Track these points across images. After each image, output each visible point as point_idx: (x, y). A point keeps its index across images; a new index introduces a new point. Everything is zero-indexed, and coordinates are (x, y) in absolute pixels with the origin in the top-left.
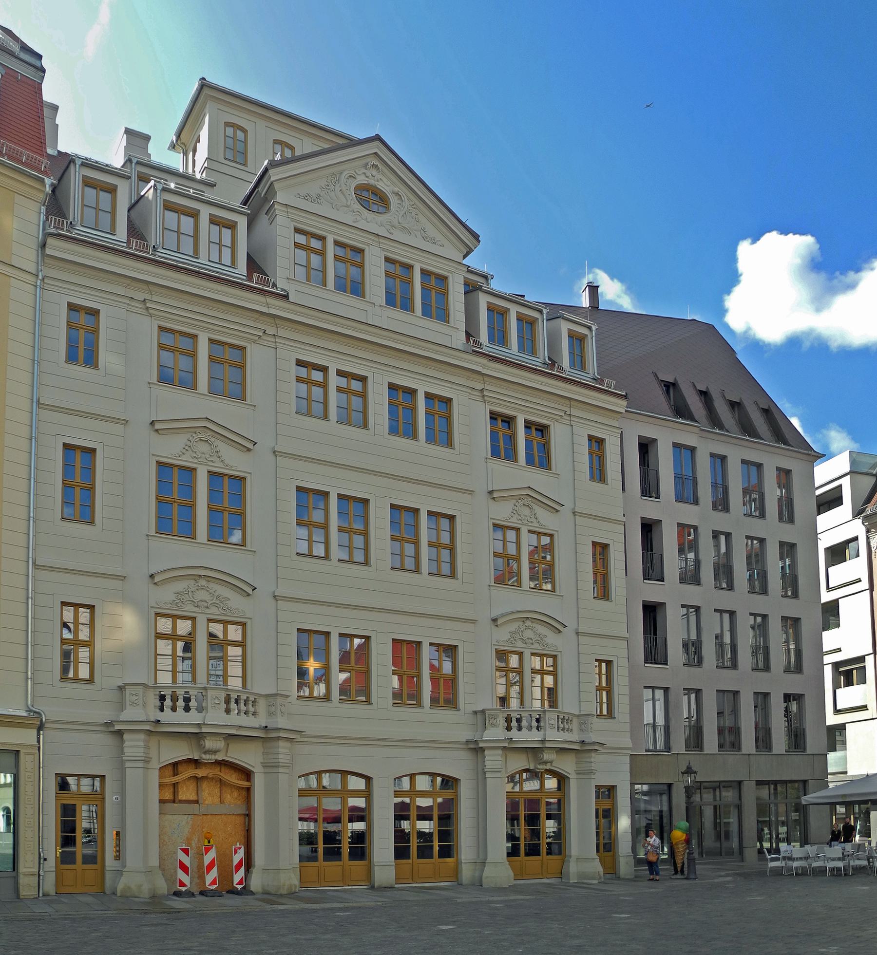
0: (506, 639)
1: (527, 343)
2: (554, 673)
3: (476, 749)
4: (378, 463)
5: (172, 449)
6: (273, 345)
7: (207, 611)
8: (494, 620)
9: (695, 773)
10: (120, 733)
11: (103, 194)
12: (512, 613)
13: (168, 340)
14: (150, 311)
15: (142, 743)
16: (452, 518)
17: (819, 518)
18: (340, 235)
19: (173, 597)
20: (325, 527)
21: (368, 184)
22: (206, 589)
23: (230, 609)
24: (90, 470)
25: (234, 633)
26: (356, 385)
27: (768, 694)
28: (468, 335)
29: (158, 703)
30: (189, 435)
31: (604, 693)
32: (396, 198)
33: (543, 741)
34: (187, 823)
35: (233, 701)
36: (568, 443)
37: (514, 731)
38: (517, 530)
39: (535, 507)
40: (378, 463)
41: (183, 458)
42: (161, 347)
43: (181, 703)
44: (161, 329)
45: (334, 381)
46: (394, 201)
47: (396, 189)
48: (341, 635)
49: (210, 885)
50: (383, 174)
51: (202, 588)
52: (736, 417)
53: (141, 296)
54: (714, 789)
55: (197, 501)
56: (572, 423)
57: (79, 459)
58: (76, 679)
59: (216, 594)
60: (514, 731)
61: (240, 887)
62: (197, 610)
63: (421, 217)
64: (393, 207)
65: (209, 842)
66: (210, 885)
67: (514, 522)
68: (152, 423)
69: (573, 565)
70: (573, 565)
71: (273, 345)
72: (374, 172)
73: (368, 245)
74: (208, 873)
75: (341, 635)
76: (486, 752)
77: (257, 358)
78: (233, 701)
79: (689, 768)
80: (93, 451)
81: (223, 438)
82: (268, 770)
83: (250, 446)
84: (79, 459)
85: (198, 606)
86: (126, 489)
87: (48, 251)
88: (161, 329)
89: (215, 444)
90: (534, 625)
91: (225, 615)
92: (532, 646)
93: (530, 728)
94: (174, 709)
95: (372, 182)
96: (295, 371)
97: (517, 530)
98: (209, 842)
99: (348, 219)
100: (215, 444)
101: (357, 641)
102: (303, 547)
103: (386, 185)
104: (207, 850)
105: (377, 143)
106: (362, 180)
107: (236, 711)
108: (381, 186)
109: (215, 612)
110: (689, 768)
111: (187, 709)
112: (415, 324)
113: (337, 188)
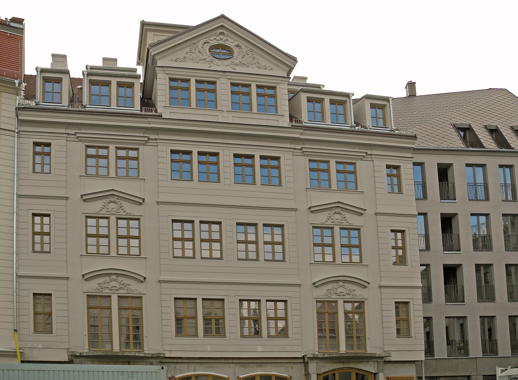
0: (324, 294)
6: (370, 159)
7: (344, 297)
8: (314, 284)
11: (339, 107)
13: (314, 165)
14: (80, 138)
16: (282, 226)
18: (171, 74)
19: (97, 286)
20: (332, 245)
22: (343, 287)
23: (131, 290)
26: (394, 172)
27: (493, 317)
28: (291, 118)
30: (329, 212)
32: (238, 48)
38: (332, 228)
39: (344, 213)
42: (311, 170)
44: (310, 161)
45: (258, 162)
46: (236, 51)
47: (237, 43)
48: (203, 299)
50: (228, 36)
51: (341, 286)
52: (494, 136)
53: (299, 147)
56: (373, 159)
59: (349, 288)
62: (111, 292)
63: (256, 56)
64: (235, 55)
67: (329, 223)
68: (309, 208)
71: (370, 159)
72: (221, 37)
73: (278, 83)
75: (203, 299)
77: (362, 166)
83: (141, 201)
87: (20, 118)
88: (310, 161)
89: (343, 214)
90: (345, 284)
91: (128, 293)
92: (344, 297)
95: (221, 42)
96: (386, 171)
97: (332, 228)
100: (120, 203)
101: (356, 304)
102: (319, 258)
103: (231, 43)
108: (227, 43)
113: (197, 51)
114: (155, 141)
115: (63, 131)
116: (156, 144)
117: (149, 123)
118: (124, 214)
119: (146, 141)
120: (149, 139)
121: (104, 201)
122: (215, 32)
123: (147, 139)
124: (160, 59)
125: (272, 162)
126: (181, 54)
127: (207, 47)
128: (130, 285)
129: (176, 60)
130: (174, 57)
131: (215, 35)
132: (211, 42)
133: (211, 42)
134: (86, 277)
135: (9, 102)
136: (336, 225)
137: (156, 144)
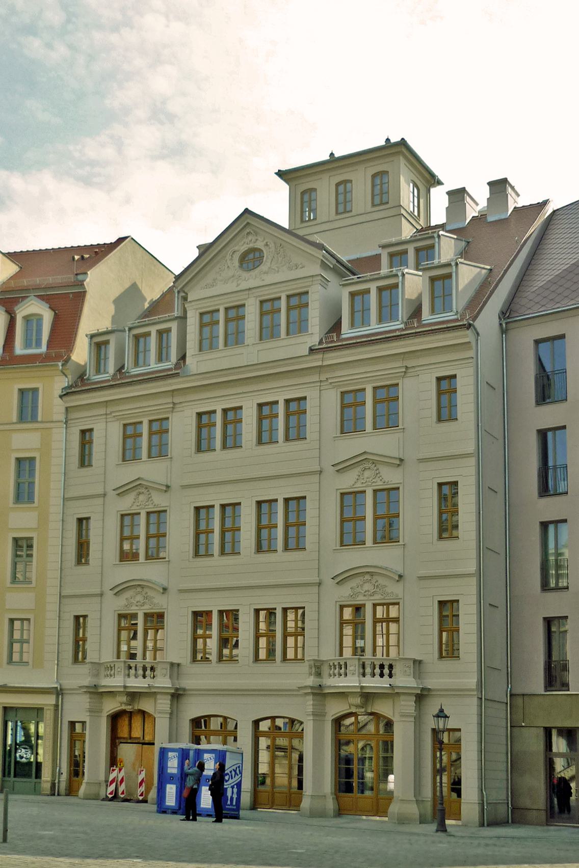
3: (319, 693)
4: (250, 472)
9: (446, 717)
12: (386, 569)
15: (475, 693)
17: (445, 221)
25: (393, 613)
29: (361, 671)
31: (81, 635)
33: (149, 687)
35: (149, 669)
36: (417, 395)
37: (368, 677)
54: (131, 738)
60: (368, 677)
62: (365, 598)
69: (418, 513)
70: (418, 513)
76: (158, 696)
78: (149, 669)
79: (441, 711)
86: (105, 539)
93: (136, 676)
94: (144, 677)
95: (251, 245)
106: (237, 264)
109: (377, 598)
110: (441, 711)
111: (382, 675)
118: (381, 483)
120: (407, 367)
125: (296, 408)
126: (209, 279)
129: (207, 286)
131: (243, 237)
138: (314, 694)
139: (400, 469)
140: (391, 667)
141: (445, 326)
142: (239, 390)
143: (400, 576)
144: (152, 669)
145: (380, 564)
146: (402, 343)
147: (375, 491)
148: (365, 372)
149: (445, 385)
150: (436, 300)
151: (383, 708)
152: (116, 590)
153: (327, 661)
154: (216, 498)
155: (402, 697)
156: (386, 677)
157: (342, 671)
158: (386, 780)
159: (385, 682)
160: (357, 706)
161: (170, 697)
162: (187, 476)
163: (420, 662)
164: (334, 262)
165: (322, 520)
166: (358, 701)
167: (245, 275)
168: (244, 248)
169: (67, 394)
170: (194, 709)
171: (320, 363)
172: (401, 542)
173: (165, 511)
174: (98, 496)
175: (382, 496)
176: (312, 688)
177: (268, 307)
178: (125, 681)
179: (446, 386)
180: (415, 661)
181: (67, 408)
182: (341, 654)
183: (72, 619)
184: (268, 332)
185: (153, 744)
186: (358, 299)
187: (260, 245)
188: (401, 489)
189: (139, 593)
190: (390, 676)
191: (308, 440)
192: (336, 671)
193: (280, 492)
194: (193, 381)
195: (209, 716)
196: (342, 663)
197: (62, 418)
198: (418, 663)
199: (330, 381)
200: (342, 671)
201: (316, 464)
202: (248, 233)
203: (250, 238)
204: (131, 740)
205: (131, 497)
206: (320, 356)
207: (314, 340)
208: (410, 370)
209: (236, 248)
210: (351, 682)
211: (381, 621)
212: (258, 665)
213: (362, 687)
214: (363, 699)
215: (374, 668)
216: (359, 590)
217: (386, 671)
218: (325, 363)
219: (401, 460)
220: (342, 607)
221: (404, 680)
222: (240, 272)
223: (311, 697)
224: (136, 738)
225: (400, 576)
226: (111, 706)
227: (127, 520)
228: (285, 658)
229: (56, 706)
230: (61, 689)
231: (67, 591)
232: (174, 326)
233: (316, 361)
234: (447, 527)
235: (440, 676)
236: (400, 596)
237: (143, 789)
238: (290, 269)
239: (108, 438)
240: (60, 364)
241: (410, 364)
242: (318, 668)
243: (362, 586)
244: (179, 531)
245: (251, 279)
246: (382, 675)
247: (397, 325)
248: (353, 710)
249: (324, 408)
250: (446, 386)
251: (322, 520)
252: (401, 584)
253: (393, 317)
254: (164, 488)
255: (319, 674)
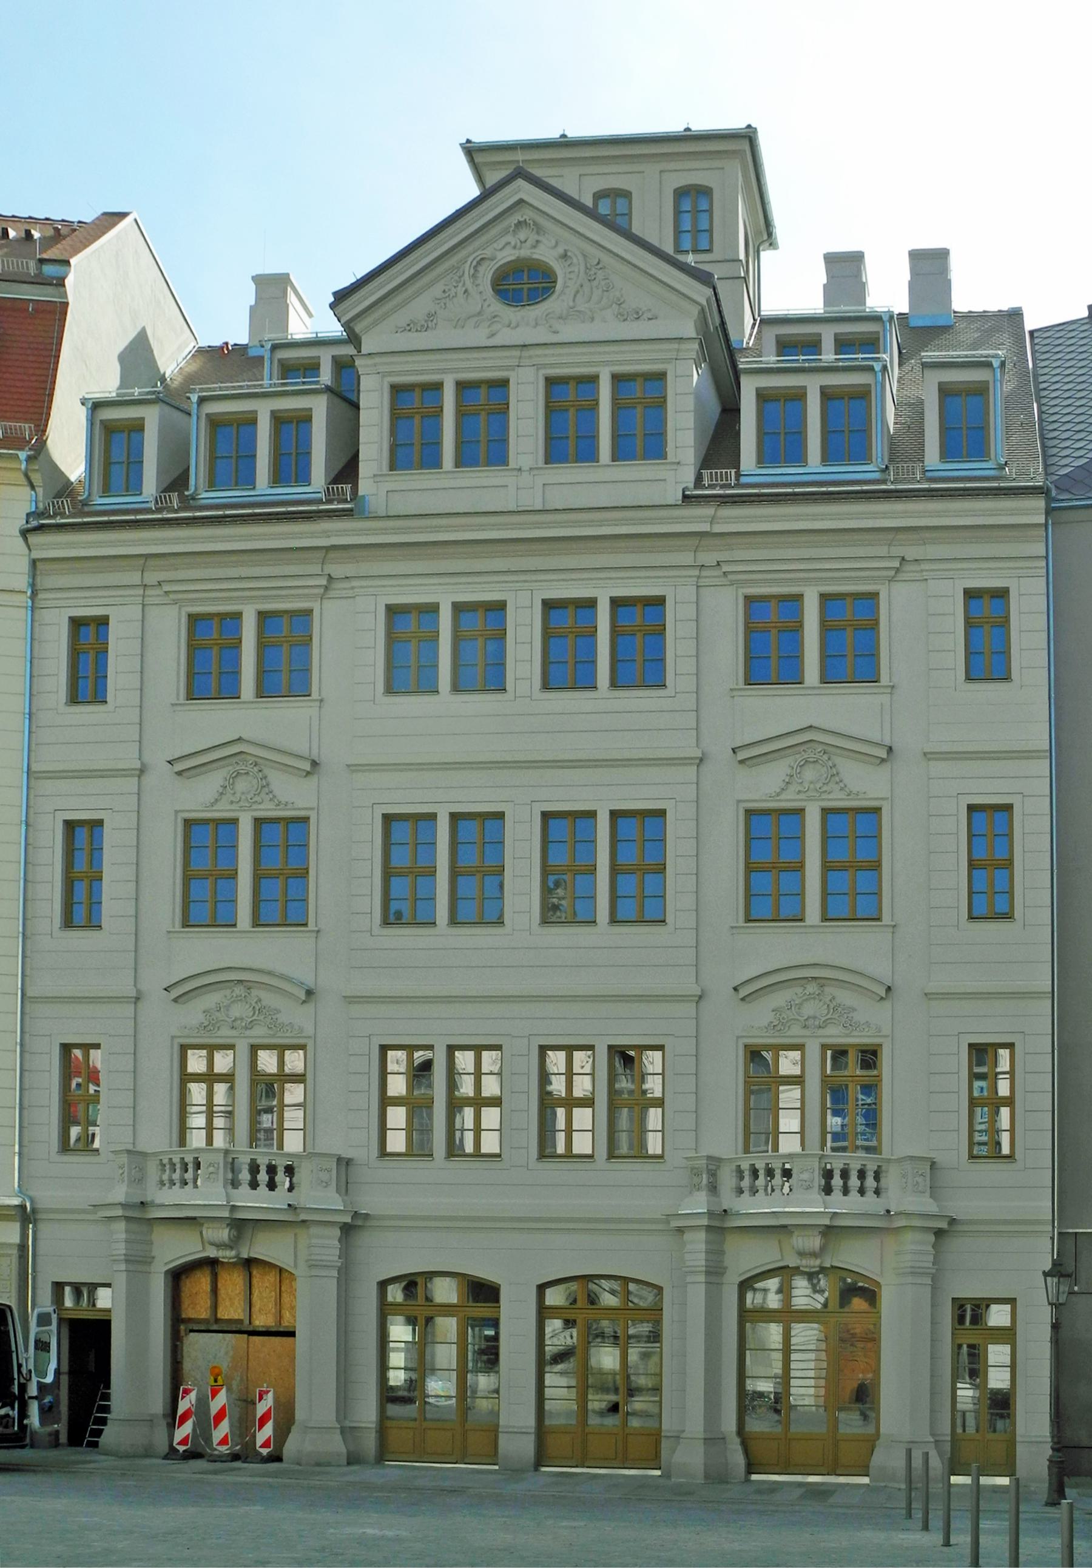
1: (118, 473)
2: (186, 1078)
4: (520, 747)
5: (767, 786)
10: (680, 1230)
12: (270, 973)
14: (172, 596)
21: (518, 260)
24: (96, 850)
25: (295, 1061)
29: (230, 1176)
34: (227, 1353)
36: (920, 622)
40: (520, 747)
41: (782, 797)
43: (263, 1177)
49: (179, 1444)
54: (217, 1321)
55: (237, 867)
57: (82, 836)
58: (556, 1156)
60: (245, 1189)
61: (265, 1451)
62: (234, 1033)
65: (216, 1381)
66: (179, 1444)
69: (923, 859)
70: (923, 859)
74: (216, 1427)
80: (1008, 808)
81: (214, 765)
82: (131, 1268)
84: (82, 836)
85: (805, 1027)
86: (142, 871)
95: (525, 252)
98: (216, 1381)
99: (479, 337)
104: (215, 1393)
105: (520, 182)
107: (287, 1185)
109: (260, 1033)
111: (254, 1185)
112: (605, 483)
114: (918, 568)
115: (687, 558)
116: (350, 593)
117: (327, 534)
118: (842, 795)
119: (898, 570)
120: (330, 578)
121: (790, 760)
122: (505, 224)
123: (897, 564)
124: (368, 329)
125: (642, 623)
126: (420, 306)
127: (486, 274)
128: (854, 1010)
129: (409, 327)
130: (402, 318)
131: (506, 232)
132: (500, 255)
133: (500, 255)
134: (743, 992)
135: (20, 502)
136: (810, 799)
137: (350, 593)
138: (128, 1219)
139: (886, 768)
140: (290, 1170)
141: (106, 518)
142: (420, 567)
143: (309, 993)
144: (290, 1170)
145: (280, 968)
146: (899, 506)
147: (826, 812)
148: (808, 554)
149: (565, 619)
150: (115, 469)
151: (858, 1258)
152: (175, 993)
153: (154, 1154)
154: (442, 797)
155: (314, 1230)
156: (870, 1195)
157: (189, 1176)
158: (761, 1395)
159: (869, 1203)
160: (219, 1246)
161: (337, 1232)
162: (362, 742)
163: (348, 1162)
164: (718, 321)
165: (705, 864)
166: (223, 1234)
167: (509, 313)
168: (507, 256)
169: (40, 528)
170: (389, 1257)
171: (705, 527)
172: (311, 926)
173: (306, 820)
174: (683, 761)
175: (469, 830)
176: (124, 1206)
177: (568, 397)
178: (228, 1197)
179: (986, 610)
180: (339, 1159)
181: (34, 563)
182: (182, 1142)
183: (56, 1051)
184: (567, 443)
185: (292, 1334)
186: (120, 439)
187: (546, 254)
188: (885, 813)
189: (811, 997)
190: (877, 1192)
191: (110, 706)
192: (176, 1176)
193: (602, 796)
194: (385, 531)
195: (431, 1275)
196: (189, 1159)
197: (22, 582)
198: (345, 1163)
199: (167, 588)
200: (189, 1176)
201: (695, 744)
202: (519, 224)
203: (522, 235)
204: (216, 1326)
205: (214, 780)
206: (708, 511)
207: (687, 476)
208: (908, 567)
209: (488, 252)
210: (208, 1194)
211: (197, 1078)
212: (549, 1165)
213: (234, 1208)
214: (234, 1232)
215: (742, 1178)
216: (221, 1016)
217: (870, 1182)
218: (718, 529)
219: (315, 764)
220: (184, 1049)
221: (903, 1196)
222: (496, 306)
223: (122, 1226)
224: (230, 1321)
225: (309, 993)
226: (176, 1248)
227: (401, 832)
228: (454, 1150)
229: (22, 1247)
230: (34, 1210)
231: (42, 986)
232: (319, 408)
233: (698, 520)
234: (989, 889)
235: (979, 1193)
236: (309, 1030)
237: (268, 1430)
238: (623, 317)
239: (148, 646)
240: (23, 455)
241: (911, 553)
242: (709, 1172)
243: (228, 1007)
244: (344, 869)
245: (523, 324)
246: (254, 1185)
247: (868, 471)
248: (212, 1253)
249: (705, 629)
250: (986, 610)
251: (705, 864)
252: (309, 1008)
253: (863, 455)
254: (307, 766)
255: (139, 1180)
